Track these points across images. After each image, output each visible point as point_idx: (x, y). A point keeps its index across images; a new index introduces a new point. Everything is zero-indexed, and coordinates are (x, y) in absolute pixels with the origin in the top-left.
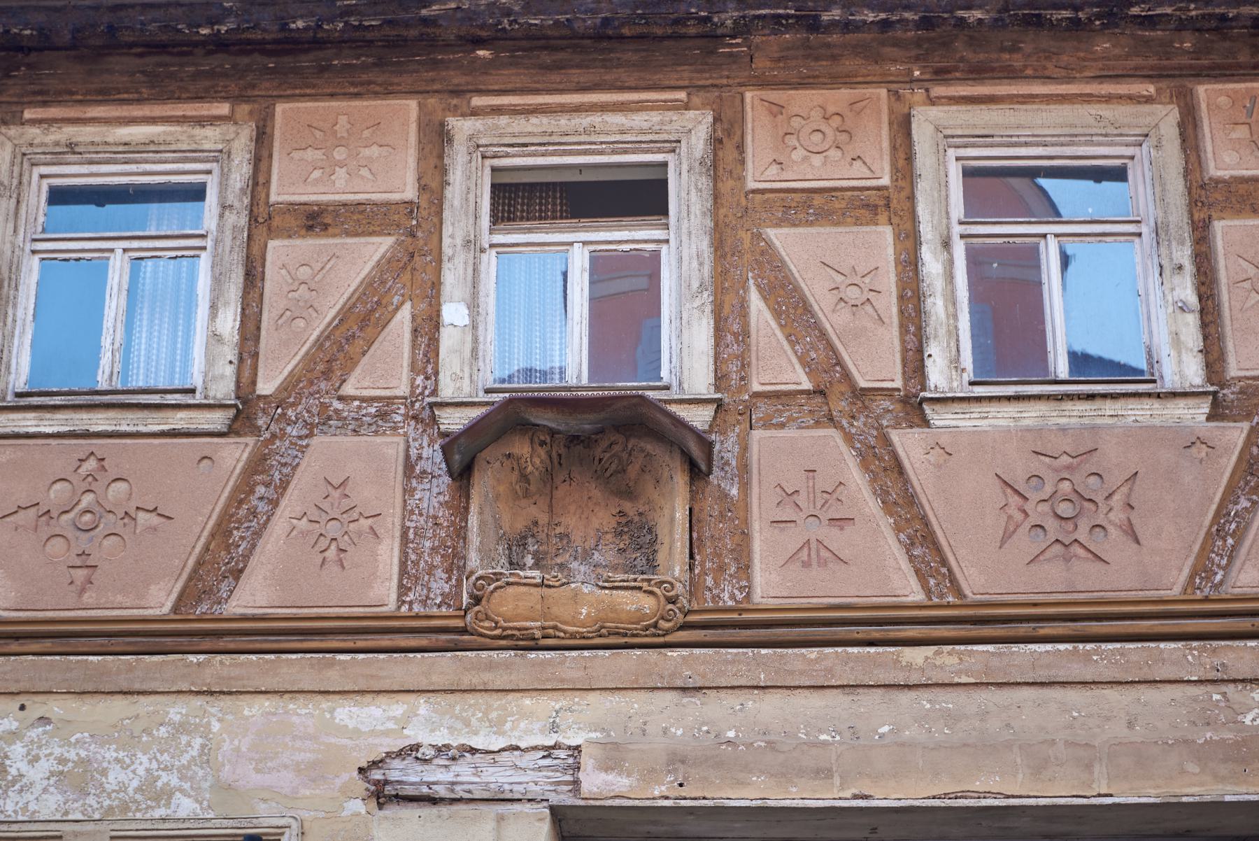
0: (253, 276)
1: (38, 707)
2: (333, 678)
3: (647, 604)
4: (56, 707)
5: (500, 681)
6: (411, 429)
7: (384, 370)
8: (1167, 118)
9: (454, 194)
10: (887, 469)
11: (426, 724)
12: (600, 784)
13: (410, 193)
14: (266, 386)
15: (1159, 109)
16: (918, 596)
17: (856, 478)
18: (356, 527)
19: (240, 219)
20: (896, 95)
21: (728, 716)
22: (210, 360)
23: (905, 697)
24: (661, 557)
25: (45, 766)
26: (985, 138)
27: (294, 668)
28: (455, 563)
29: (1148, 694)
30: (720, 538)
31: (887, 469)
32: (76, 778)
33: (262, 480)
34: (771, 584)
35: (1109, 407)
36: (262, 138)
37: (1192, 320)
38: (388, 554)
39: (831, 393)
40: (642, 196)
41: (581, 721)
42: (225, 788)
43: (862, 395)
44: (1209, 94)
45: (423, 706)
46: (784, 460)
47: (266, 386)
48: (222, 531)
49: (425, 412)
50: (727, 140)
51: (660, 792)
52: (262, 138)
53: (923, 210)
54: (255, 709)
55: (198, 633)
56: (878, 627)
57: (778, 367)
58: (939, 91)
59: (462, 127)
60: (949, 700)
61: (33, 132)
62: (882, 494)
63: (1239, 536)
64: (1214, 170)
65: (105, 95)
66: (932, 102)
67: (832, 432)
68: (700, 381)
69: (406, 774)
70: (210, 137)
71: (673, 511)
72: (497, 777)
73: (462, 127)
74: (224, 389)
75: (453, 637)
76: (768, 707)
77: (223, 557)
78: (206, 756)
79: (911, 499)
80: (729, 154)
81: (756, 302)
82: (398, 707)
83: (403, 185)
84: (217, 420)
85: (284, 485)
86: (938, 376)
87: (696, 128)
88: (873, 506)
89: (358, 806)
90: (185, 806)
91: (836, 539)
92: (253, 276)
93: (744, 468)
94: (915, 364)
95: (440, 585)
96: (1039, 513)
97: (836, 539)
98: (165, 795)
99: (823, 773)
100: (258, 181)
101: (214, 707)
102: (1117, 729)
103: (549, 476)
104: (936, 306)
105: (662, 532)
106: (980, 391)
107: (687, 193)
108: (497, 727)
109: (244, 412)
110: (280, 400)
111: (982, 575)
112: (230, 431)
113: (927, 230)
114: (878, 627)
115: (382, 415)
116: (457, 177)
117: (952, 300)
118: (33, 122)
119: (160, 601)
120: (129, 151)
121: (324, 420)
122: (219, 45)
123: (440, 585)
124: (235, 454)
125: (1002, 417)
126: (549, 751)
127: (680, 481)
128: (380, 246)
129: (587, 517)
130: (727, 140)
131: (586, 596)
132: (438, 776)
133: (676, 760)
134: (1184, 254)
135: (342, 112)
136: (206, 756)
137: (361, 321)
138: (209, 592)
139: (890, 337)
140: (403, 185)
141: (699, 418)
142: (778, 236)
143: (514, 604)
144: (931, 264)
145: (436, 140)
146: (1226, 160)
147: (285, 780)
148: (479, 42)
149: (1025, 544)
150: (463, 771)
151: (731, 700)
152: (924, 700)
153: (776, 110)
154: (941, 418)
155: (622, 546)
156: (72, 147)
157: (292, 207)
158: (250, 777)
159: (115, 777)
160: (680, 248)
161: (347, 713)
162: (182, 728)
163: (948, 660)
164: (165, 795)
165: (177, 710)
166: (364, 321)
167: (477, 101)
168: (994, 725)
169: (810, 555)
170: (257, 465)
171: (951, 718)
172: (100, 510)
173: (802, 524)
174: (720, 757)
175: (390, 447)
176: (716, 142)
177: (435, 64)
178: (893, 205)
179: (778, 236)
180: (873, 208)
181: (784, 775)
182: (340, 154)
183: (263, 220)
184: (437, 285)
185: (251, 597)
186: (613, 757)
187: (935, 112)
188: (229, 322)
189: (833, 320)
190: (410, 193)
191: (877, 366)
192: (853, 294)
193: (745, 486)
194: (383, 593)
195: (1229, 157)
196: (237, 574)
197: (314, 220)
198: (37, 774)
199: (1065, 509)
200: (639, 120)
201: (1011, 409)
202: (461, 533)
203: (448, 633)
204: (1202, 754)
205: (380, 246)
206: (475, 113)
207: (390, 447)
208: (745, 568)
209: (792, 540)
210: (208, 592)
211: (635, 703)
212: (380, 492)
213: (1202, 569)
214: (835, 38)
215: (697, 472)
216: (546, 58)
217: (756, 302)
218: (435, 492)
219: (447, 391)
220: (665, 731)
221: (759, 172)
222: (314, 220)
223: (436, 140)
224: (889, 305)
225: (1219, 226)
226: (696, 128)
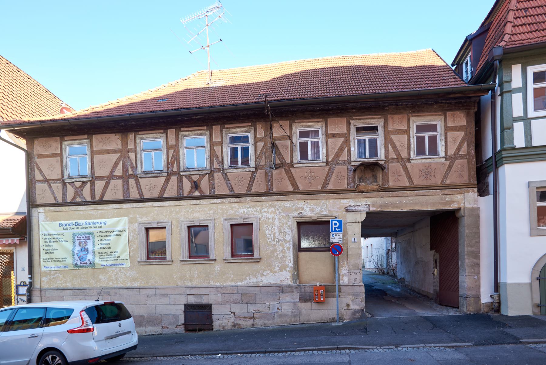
0: (327, 144)
1: (306, 201)
2: (341, 197)
3: (377, 187)
4: (308, 201)
5: (360, 197)
6: (347, 164)
7: (344, 157)
8: (442, 118)
9: (351, 132)
10: (405, 168)
11: (352, 202)
12: (372, 209)
13: (346, 132)
14: (330, 160)
15: (442, 116)
16: (409, 185)
17: (402, 170)
18: (342, 177)
19: (324, 136)
20: (408, 115)
21: (387, 200)
22: (323, 156)
23: (407, 198)
24: (378, 180)
25: (308, 208)
26: (419, 121)
27: (336, 195)
28: (354, 182)
29: (435, 196)
30: (385, 179)
31: (405, 168)
32: (312, 210)
33: (330, 172)
34: (391, 184)
35: (433, 160)
36: (326, 124)
37: (444, 147)
38: (346, 181)
39: (399, 159)
40: (375, 129)
41: (369, 201)
42: (329, 211)
43: (402, 158)
44: (449, 114)
45: (351, 200)
46: (394, 167)
47: (330, 160)
48: (326, 179)
49: (349, 162)
50: (386, 123)
51: (379, 210)
52: (326, 124)
53: (411, 133)
54: (332, 201)
55: (324, 192)
56: (404, 189)
57: (393, 156)
58: (413, 115)
59: (352, 122)
60: (412, 198)
61: (297, 124)
62: (405, 172)
63: (447, 176)
64: (448, 125)
65: (306, 118)
66: (413, 116)
67: (399, 164)
68: (383, 157)
69: (349, 208)
70: (320, 124)
71: (380, 175)
72: (360, 208)
73: (352, 122)
74: (325, 160)
75: (354, 191)
76: (391, 199)
77: (326, 182)
78: (327, 207)
79: (408, 172)
80: (386, 124)
81: (390, 146)
82: (348, 200)
83: (345, 131)
84: (324, 164)
85: (333, 172)
86: (412, 156)
87: (382, 121)
88: (403, 173)
89: (345, 212)
90: (325, 213)
91: (399, 178)
92: (327, 144)
93: (388, 169)
94: (409, 154)
95: (352, 185)
96: (424, 174)
97: (399, 178)
98: (322, 212)
99: (397, 207)
100: (326, 130)
101: (327, 201)
102: (431, 201)
103: (364, 170)
104: (412, 146)
105: (378, 177)
106: (417, 157)
107: (381, 130)
108: (360, 202)
109: (327, 163)
110: (332, 161)
111: (417, 182)
112: (326, 166)
113: (411, 135)
114: (404, 189)
115: (344, 163)
116: (352, 129)
117: (414, 145)
118: (297, 122)
119: (319, 188)
120: (310, 126)
121: (337, 164)
122: (320, 110)
123: (352, 185)
124: (327, 168)
125: (420, 161)
126: (366, 205)
127: (381, 171)
128: (342, 139)
129: (369, 175)
130: (386, 123)
131: (370, 187)
132: (353, 208)
133: (381, 206)
134: (443, 138)
135: (336, 120)
136: (327, 207)
137: (341, 150)
138: (325, 186)
139: (406, 151)
140: (345, 131)
141: (382, 162)
142: (392, 136)
143: (361, 188)
144: (412, 140)
145: (349, 124)
146: (450, 124)
147: (336, 210)
148: (354, 109)
149: (422, 178)
150: (356, 208)
151: (386, 198)
152: (409, 198)
153: (392, 118)
154: (412, 162)
155: (79, 263)
156: (302, 126)
157: (331, 134)
158: (333, 210)
159: (317, 210)
160: (380, 138)
161: (342, 201)
162: (324, 203)
163: (412, 193)
164: (322, 212)
165: (323, 201)
166: (341, 150)
167: (354, 118)
168: (417, 201)
169: (396, 180)
170: (330, 170)
171: (412, 200)
172: (311, 176)
173: (396, 176)
174: (386, 206)
175: (345, 167)
176: (385, 123)
177: (348, 112)
178: (407, 132)
179: (392, 136)
180: (404, 132)
181: (393, 207)
182: (336, 126)
183: (447, 129)
184: (350, 145)
185: (330, 187)
186: (373, 206)
187: (413, 118)
188: (325, 151)
189: (399, 148)
190: (346, 132)
191: (404, 155)
192: (402, 145)
193: (388, 171)
194: (346, 186)
195: (450, 123)
196: (328, 184)
197: (334, 136)
198: (307, 209)
199: (427, 173)
200: (375, 120)
201: (421, 160)
202: (354, 178)
203: (354, 191)
204: (441, 204)
205: (342, 139)
206: (353, 119)
207: (345, 167)
208: (388, 182)
209: (394, 178)
210: (325, 186)
211: (375, 199)
212: (345, 174)
213: (443, 181)
214: (400, 106)
215: (382, 170)
216: (362, 111)
217: (390, 146)
218: (351, 173)
219: (352, 160)
220: (348, 305)
221: (390, 128)
222: (334, 136)
223: (349, 124)
224: (406, 146)
225: (448, 133)
226: (382, 121)
